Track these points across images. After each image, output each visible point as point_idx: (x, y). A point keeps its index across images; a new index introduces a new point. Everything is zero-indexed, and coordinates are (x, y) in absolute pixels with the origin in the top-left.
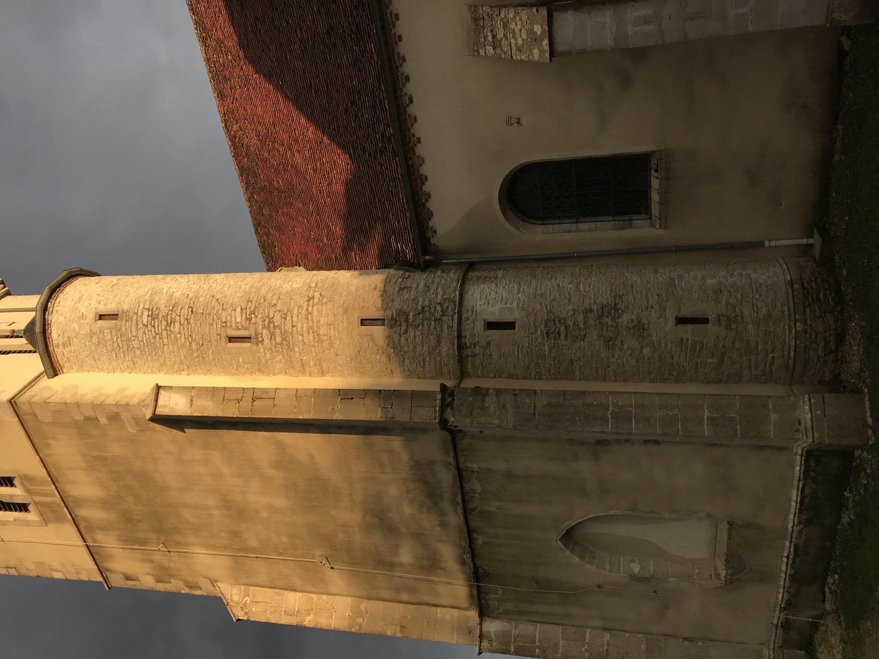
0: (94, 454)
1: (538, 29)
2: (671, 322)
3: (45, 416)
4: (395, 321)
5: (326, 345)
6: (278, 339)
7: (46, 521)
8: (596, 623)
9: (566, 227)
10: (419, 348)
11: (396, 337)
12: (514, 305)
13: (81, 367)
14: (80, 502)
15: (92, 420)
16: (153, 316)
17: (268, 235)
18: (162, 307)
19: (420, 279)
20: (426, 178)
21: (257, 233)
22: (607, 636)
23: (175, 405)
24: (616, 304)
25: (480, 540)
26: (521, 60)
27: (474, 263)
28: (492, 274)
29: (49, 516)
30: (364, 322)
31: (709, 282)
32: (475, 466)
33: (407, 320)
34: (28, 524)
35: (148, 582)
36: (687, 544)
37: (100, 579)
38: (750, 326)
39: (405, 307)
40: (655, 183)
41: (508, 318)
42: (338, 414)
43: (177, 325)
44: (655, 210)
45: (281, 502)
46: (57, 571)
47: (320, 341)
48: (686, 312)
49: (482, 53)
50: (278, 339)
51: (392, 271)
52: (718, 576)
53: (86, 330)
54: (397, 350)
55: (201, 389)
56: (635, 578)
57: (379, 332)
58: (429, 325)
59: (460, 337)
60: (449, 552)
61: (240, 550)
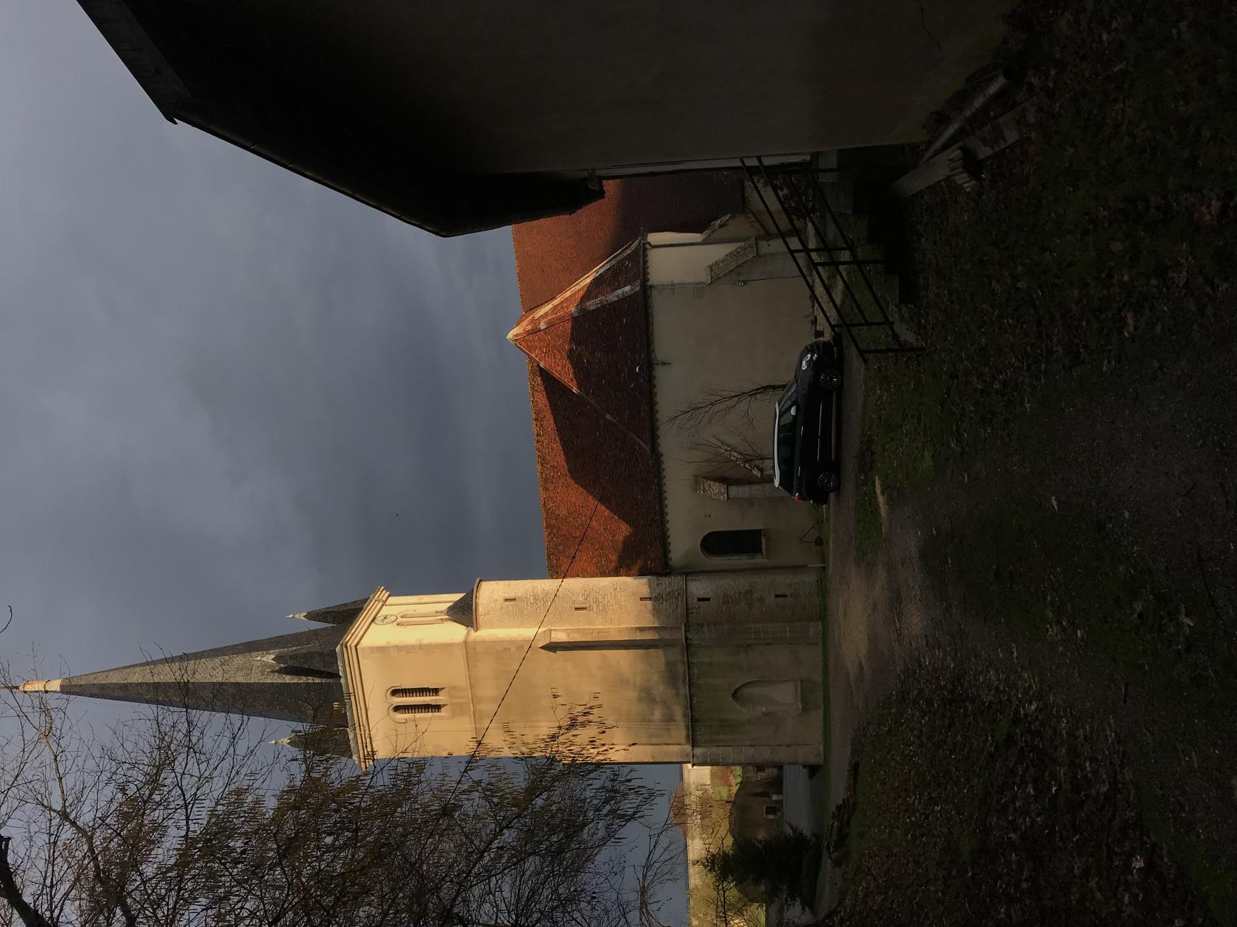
4: (655, 598)
7: (453, 715)
8: (748, 743)
13: (492, 625)
16: (536, 599)
19: (666, 580)
23: (560, 637)
25: (695, 700)
27: (689, 572)
29: (459, 710)
30: (641, 599)
34: (442, 718)
36: (784, 695)
42: (639, 636)
54: (657, 612)
57: (649, 603)
60: (678, 712)
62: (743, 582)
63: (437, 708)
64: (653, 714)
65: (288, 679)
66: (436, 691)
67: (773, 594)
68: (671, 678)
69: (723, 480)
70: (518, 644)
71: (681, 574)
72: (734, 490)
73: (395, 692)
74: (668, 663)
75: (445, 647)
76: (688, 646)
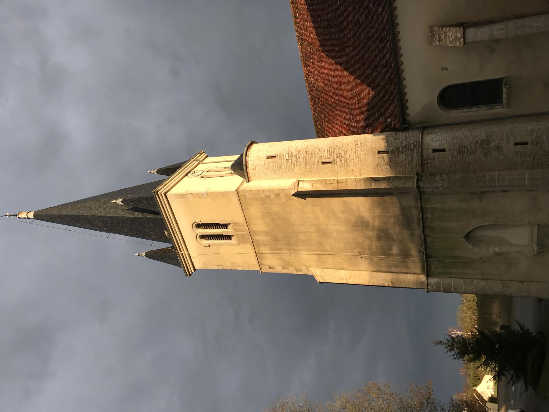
0: (266, 211)
1: (459, 35)
2: (512, 144)
3: (249, 196)
4: (391, 152)
5: (363, 163)
6: (343, 162)
7: (239, 243)
9: (465, 110)
10: (404, 162)
11: (394, 158)
12: (445, 142)
13: (259, 178)
14: (256, 233)
15: (268, 197)
17: (321, 125)
18: (294, 152)
20: (407, 93)
21: (316, 125)
22: (484, 282)
23: (306, 187)
24: (488, 139)
26: (451, 46)
27: (425, 127)
28: (434, 131)
29: (242, 240)
30: (379, 153)
31: (529, 128)
32: (429, 207)
33: (399, 151)
35: (279, 269)
37: (259, 269)
38: (546, 145)
39: (398, 146)
40: (504, 90)
41: (442, 147)
42: (374, 186)
43: (301, 159)
44: (505, 101)
45: (342, 228)
46: (240, 266)
47: (361, 161)
48: (518, 140)
49: (434, 44)
50: (343, 162)
51: (389, 133)
52: (534, 251)
53: (263, 163)
54: (392, 163)
55: (316, 180)
56: (497, 254)
58: (408, 152)
59: (422, 156)
61: (321, 251)
62: (481, 132)
63: (229, 237)
64: (391, 249)
65: (136, 215)
66: (225, 226)
67: (512, 142)
68: (406, 221)
69: (464, 25)
70: (278, 194)
71: (419, 128)
72: (472, 33)
73: (199, 226)
74: (403, 209)
75: (224, 194)
76: (421, 193)
